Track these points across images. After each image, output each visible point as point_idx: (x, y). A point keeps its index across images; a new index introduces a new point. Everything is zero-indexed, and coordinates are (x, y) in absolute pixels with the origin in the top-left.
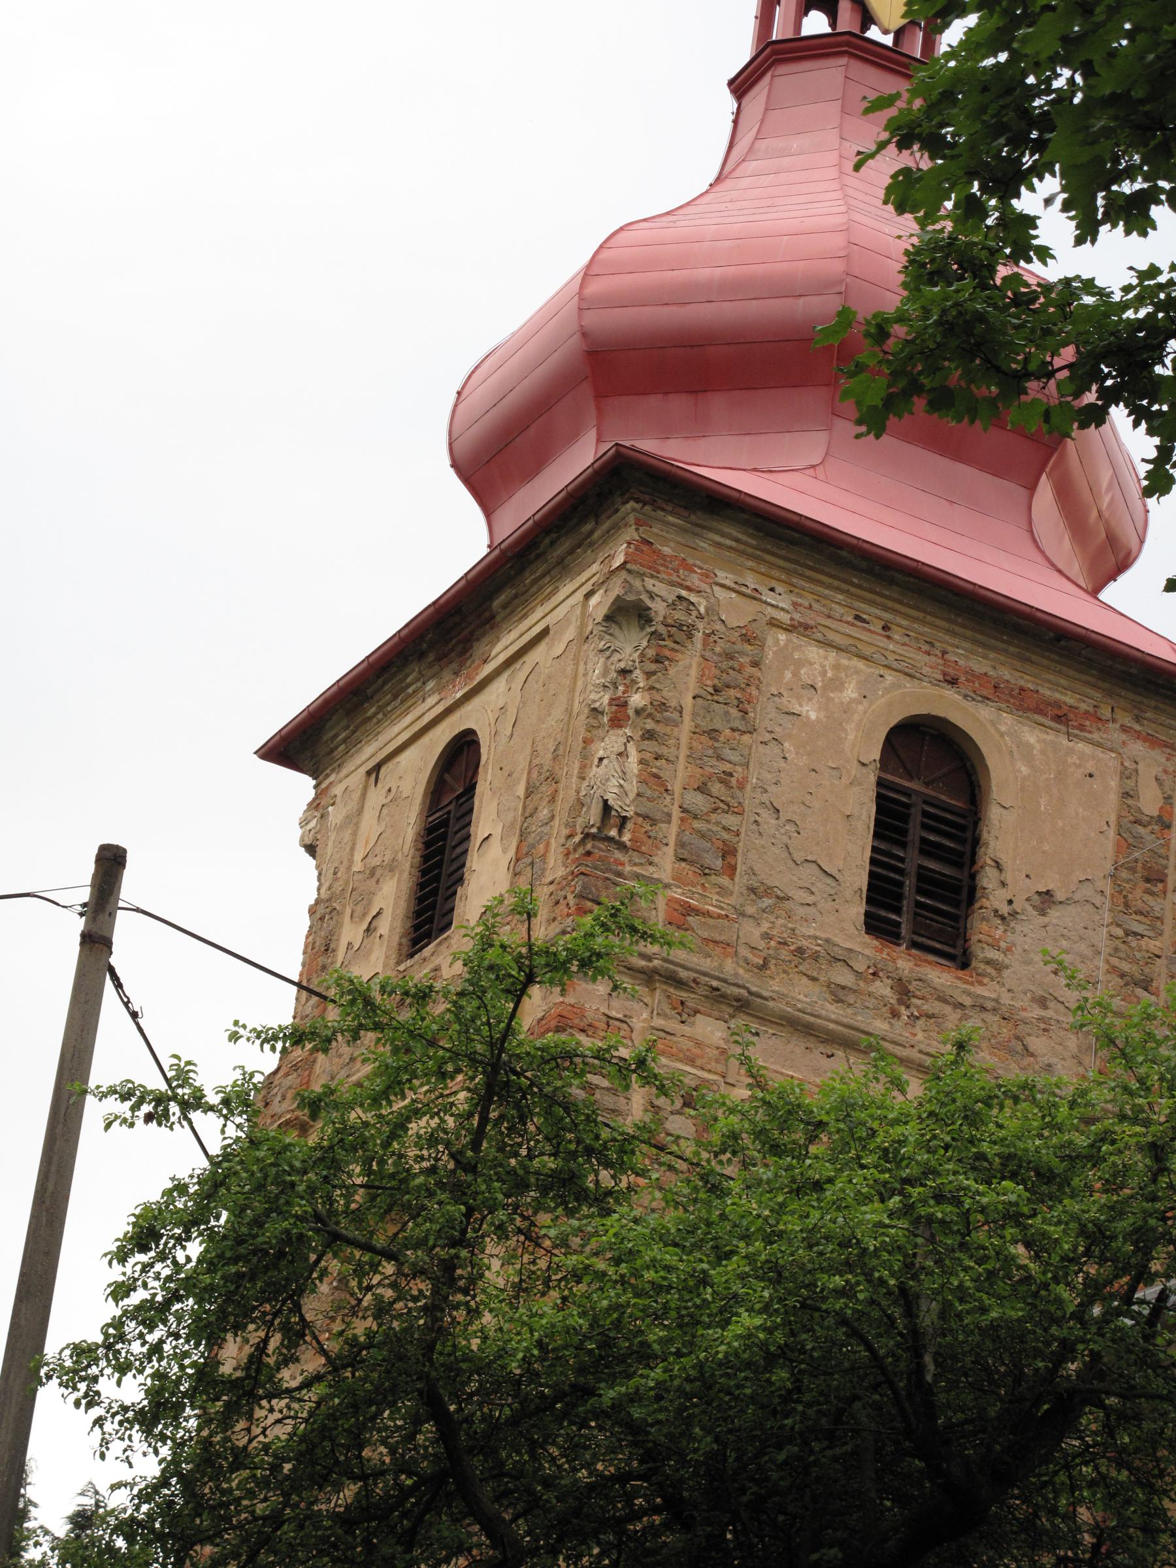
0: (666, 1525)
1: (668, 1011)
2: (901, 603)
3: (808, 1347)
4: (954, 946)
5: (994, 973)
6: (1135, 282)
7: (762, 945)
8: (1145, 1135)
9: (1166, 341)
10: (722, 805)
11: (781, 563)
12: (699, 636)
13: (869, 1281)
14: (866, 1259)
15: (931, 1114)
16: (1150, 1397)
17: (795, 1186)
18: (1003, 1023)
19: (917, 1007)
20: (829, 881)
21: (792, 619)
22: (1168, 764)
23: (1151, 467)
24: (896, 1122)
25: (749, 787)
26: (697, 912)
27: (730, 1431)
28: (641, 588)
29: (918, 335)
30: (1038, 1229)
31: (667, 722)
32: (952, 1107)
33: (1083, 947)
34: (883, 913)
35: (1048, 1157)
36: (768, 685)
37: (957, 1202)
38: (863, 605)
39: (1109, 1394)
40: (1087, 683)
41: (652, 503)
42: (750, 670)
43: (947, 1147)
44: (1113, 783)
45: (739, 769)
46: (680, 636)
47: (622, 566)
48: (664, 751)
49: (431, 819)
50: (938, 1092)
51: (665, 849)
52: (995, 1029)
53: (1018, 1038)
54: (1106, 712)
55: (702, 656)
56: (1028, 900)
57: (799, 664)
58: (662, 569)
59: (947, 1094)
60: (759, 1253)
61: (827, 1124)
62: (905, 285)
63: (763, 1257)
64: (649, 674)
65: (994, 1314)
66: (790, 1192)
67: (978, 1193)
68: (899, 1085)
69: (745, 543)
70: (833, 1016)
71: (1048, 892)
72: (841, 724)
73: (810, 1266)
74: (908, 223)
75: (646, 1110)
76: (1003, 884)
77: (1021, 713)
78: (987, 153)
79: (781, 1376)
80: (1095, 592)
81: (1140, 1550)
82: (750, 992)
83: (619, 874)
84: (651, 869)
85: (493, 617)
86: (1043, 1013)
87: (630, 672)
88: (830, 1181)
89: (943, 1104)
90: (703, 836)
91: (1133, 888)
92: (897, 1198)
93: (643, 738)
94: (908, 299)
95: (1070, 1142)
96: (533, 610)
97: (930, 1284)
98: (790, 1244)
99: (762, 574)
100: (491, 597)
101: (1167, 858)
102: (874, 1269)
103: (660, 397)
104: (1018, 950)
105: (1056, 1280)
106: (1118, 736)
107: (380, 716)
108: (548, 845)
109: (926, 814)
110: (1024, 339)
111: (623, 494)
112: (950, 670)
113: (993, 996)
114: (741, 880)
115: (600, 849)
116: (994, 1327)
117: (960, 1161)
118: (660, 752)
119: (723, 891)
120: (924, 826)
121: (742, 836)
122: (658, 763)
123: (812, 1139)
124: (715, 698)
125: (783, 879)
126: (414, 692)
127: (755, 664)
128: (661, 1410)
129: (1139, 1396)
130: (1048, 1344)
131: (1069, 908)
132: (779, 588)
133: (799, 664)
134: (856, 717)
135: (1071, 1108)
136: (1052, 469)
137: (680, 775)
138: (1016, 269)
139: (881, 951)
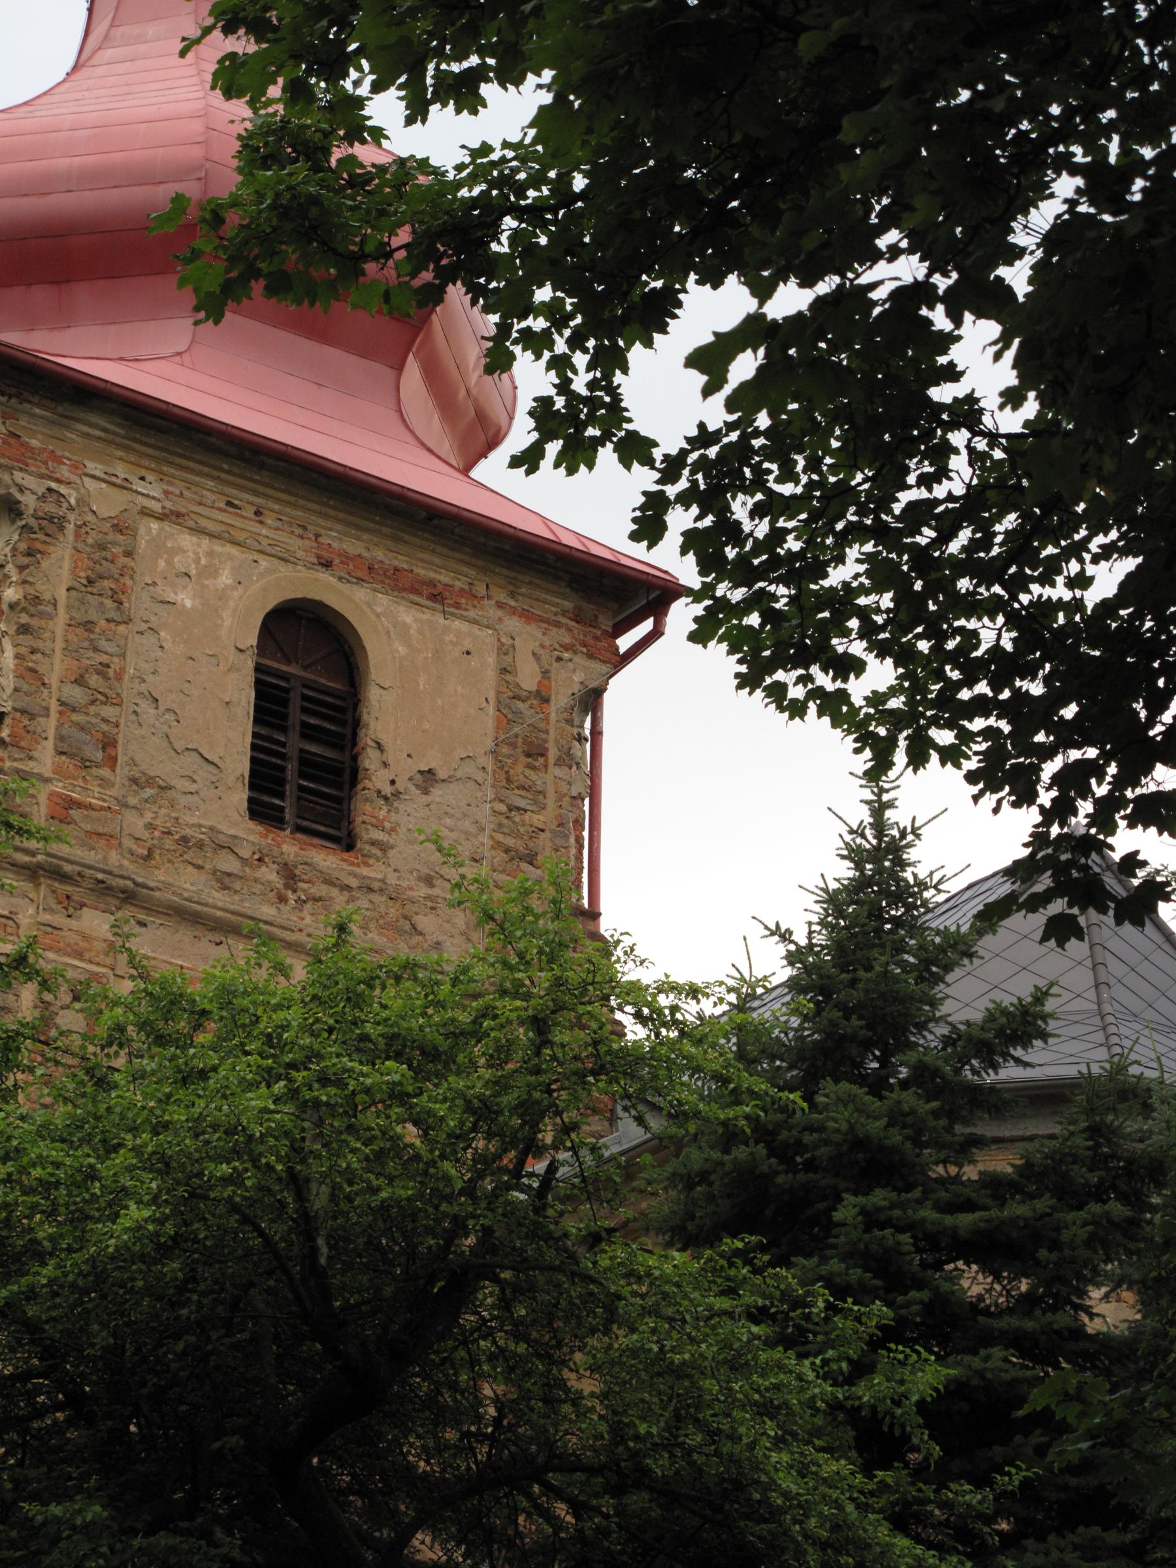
0: (69, 1422)
1: (54, 906)
2: (273, 487)
3: (201, 1236)
4: (338, 829)
5: (379, 853)
6: (467, 160)
7: (146, 835)
8: (526, 1009)
9: (501, 218)
10: (100, 697)
11: (151, 451)
12: (70, 528)
13: (255, 1166)
14: (253, 1146)
15: (315, 997)
16: (542, 1269)
17: (180, 1076)
18: (391, 903)
19: (304, 891)
20: (211, 768)
22: (545, 638)
23: (491, 344)
24: (278, 1007)
25: (126, 677)
26: (79, 805)
27: (127, 1325)
29: (252, 220)
30: (422, 1108)
31: (41, 615)
32: (335, 990)
33: (467, 825)
34: (266, 799)
35: (432, 1036)
36: (143, 574)
37: (340, 1084)
39: (504, 1268)
40: (461, 561)
41: (18, 396)
42: (123, 560)
43: (330, 1030)
44: (491, 660)
45: (116, 660)
46: (51, 529)
48: (39, 644)
50: (320, 976)
51: (44, 743)
52: (383, 910)
53: (406, 917)
54: (481, 590)
55: (75, 548)
56: (410, 779)
57: (173, 552)
59: (330, 977)
60: (145, 1145)
61: (210, 1012)
62: (240, 170)
63: (150, 1149)
64: (21, 568)
65: (384, 1194)
66: (175, 1083)
67: (363, 1075)
68: (282, 969)
69: (114, 433)
70: (220, 904)
71: (430, 771)
73: (197, 1155)
74: (240, 109)
75: (35, 1007)
76: (385, 765)
78: (311, 35)
79: (173, 1267)
80: (466, 470)
81: (542, 1421)
82: (135, 883)
84: (31, 764)
86: (430, 891)
88: (215, 1069)
89: (325, 987)
90: (82, 729)
91: (515, 763)
92: (282, 1083)
94: (243, 184)
95: (453, 1020)
97: (317, 1168)
98: (176, 1134)
101: (547, 732)
102: (261, 1155)
104: (402, 830)
105: (443, 1156)
106: (493, 613)
109: (305, 698)
110: (360, 220)
113: (379, 876)
114: (122, 772)
116: (384, 1206)
117: (344, 1043)
119: (105, 783)
120: (304, 710)
121: (122, 727)
122: (34, 657)
123: (197, 1027)
125: (163, 767)
127: (129, 554)
128: (56, 1307)
129: (534, 1269)
130: (438, 1221)
131: (452, 786)
132: (150, 477)
133: (173, 552)
134: (231, 604)
135: (454, 986)
136: (420, 347)
137: (56, 668)
138: (350, 151)
139: (266, 836)
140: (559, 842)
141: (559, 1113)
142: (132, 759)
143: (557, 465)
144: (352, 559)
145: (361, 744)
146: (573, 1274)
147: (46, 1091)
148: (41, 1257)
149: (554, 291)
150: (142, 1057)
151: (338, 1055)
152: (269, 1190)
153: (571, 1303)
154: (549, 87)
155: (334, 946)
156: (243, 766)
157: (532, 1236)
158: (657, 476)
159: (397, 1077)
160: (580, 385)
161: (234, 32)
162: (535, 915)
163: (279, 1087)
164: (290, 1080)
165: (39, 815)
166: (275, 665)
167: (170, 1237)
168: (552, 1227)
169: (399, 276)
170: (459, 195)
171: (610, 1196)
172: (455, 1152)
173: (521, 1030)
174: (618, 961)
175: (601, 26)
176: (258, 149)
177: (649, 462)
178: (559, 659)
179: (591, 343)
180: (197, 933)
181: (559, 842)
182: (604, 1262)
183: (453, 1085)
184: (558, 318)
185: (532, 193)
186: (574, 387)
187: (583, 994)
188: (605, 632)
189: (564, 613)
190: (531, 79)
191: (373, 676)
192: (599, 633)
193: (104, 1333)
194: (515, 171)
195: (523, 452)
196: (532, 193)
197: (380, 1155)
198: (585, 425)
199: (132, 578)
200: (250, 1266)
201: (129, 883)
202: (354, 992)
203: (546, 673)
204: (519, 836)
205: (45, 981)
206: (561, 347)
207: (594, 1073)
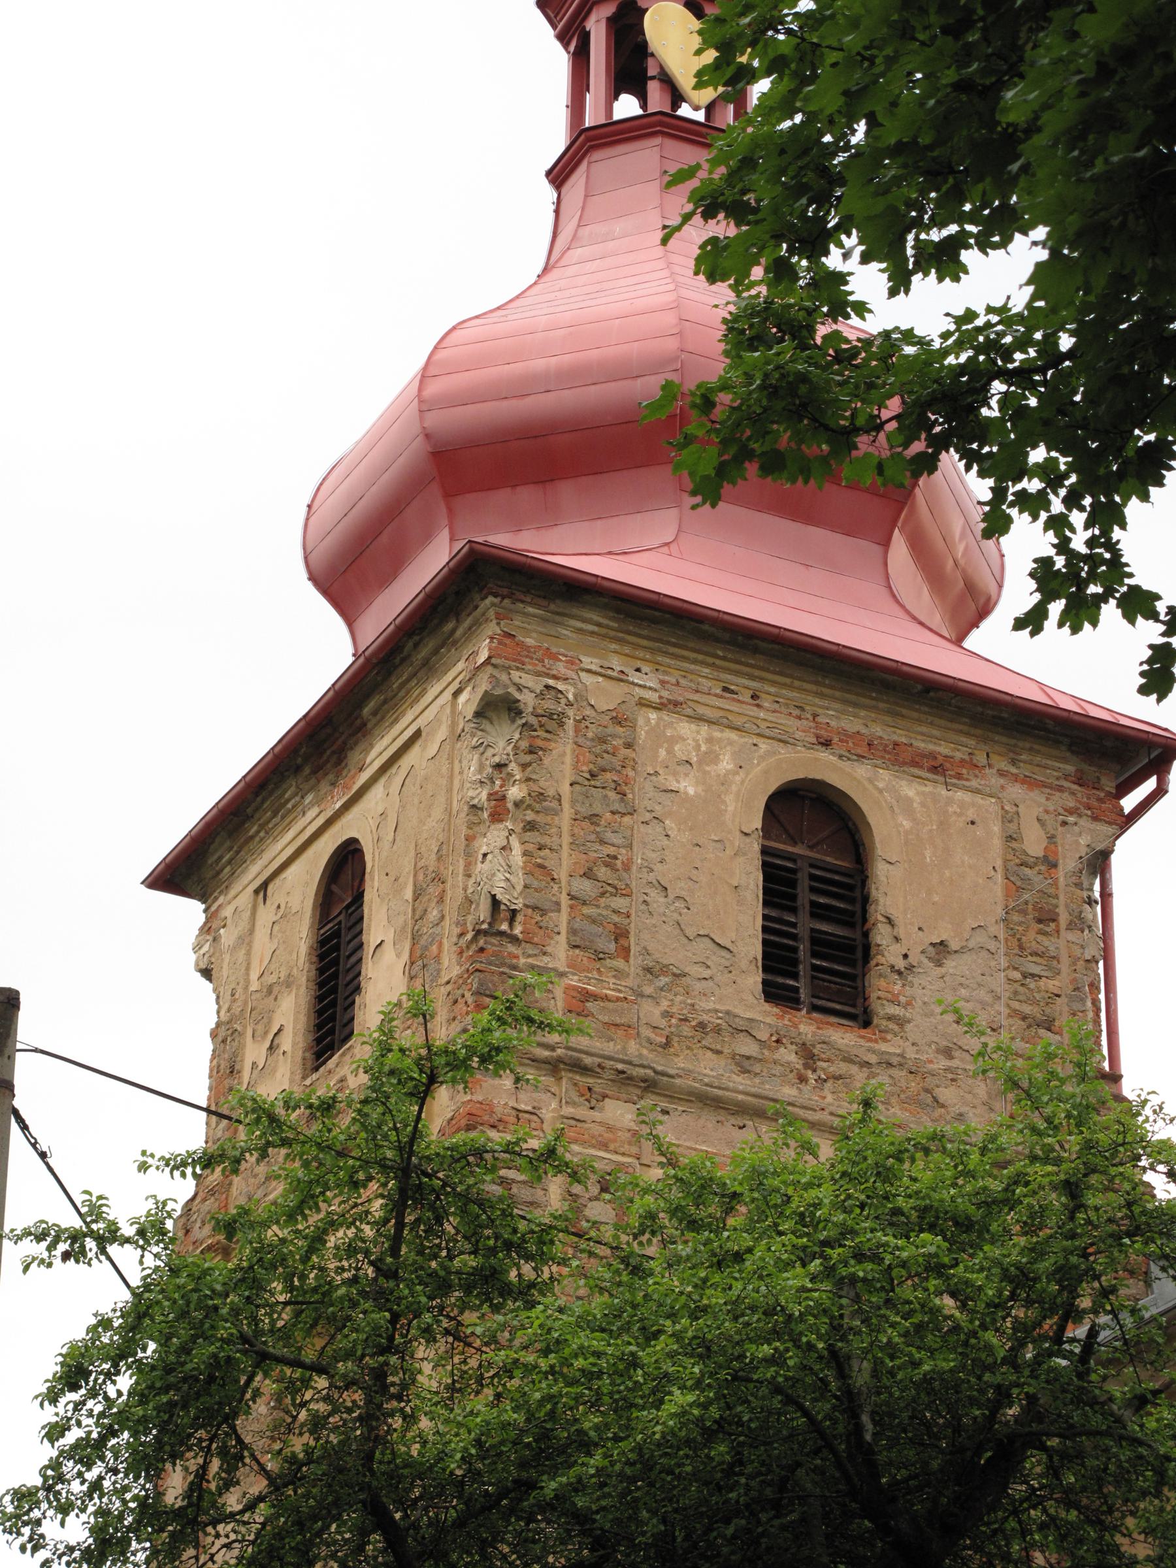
1: (576, 1099)
2: (768, 671)
3: (745, 1419)
4: (854, 1006)
5: (896, 1028)
6: (952, 327)
7: (663, 1023)
9: (989, 383)
10: (609, 889)
11: (645, 643)
12: (570, 723)
14: (793, 1326)
15: (844, 1174)
16: (1091, 1434)
17: (715, 1260)
19: (823, 1069)
20: (724, 953)
21: (661, 697)
22: (1049, 803)
23: (987, 508)
24: (809, 1186)
25: (634, 868)
26: (595, 997)
27: (676, 1511)
28: (508, 682)
31: (547, 811)
33: (982, 994)
34: (780, 980)
35: (965, 1206)
37: (876, 1258)
38: (729, 677)
39: (1049, 1435)
42: (624, 752)
43: (862, 1206)
44: (996, 828)
45: (623, 851)
46: (552, 725)
47: (488, 661)
48: (546, 840)
49: (322, 931)
50: (849, 1152)
51: (557, 938)
52: (903, 1084)
53: (927, 1091)
54: (981, 759)
55: (576, 743)
56: (922, 952)
57: (673, 740)
58: (527, 660)
59: (858, 1153)
60: (685, 1330)
62: (726, 353)
63: (690, 1334)
64: (524, 766)
65: (926, 1368)
66: (711, 1266)
67: (898, 1249)
68: (809, 1148)
69: (607, 627)
70: (741, 1087)
71: (942, 943)
72: (719, 796)
73: (737, 1338)
74: (723, 292)
76: (897, 939)
77: (897, 768)
78: (791, 214)
79: (720, 1450)
80: (959, 640)
82: (656, 1072)
83: (515, 968)
84: (546, 959)
85: (365, 725)
86: (948, 1063)
87: (505, 765)
88: (750, 1250)
89: (854, 1163)
90: (594, 921)
92: (818, 1262)
93: (525, 830)
94: (731, 367)
95: (985, 1188)
96: (403, 713)
97: (859, 1344)
98: (716, 1318)
99: (627, 655)
100: (360, 706)
101: (1056, 897)
102: (801, 1334)
103: (509, 489)
105: (984, 1327)
106: (995, 781)
107: (262, 834)
108: (440, 944)
109: (812, 877)
111: (481, 590)
112: (823, 732)
113: (898, 1051)
114: (636, 961)
115: (494, 945)
116: (927, 1379)
117: (877, 1218)
118: (542, 842)
119: (619, 974)
120: (813, 890)
122: (542, 853)
123: (729, 1210)
124: (593, 783)
125: (676, 955)
126: (293, 807)
127: (629, 746)
128: (604, 1496)
129: (1080, 1435)
130: (982, 1391)
131: (965, 956)
132: (645, 669)
133: (673, 740)
134: (734, 788)
135: (982, 1155)
137: (564, 863)
138: (835, 327)
139: (782, 1017)
140: (1076, 1006)
141: (1097, 1277)
142: (645, 948)
143: (1061, 625)
144: (850, 737)
145: (871, 920)
146: (1121, 1438)
147: (582, 1282)
148: (586, 1445)
149: (1048, 452)
150: (674, 1243)
151: (872, 1231)
152: (811, 1369)
153: (1120, 1466)
154: (1044, 244)
155: (860, 1121)
156: (755, 949)
157: (1078, 1401)
158: (1162, 628)
159: (933, 1249)
160: (1078, 543)
161: (714, 217)
162: (1059, 1079)
163: (815, 1265)
164: (826, 1258)
165: (557, 1009)
166: (781, 846)
167: (715, 1421)
168: (1097, 1392)
169: (892, 447)
170: (946, 363)
171: (1153, 1357)
172: (994, 1321)
173: (1054, 1195)
174: (1147, 1120)
175: (1093, 179)
176: (743, 331)
177: (1153, 615)
178: (1064, 823)
179: (1087, 501)
180: (720, 1118)
181: (1076, 1006)
182: (1151, 1424)
183: (990, 1254)
184: (1052, 477)
185: (1018, 356)
186: (1073, 545)
187: (1113, 1156)
188: (1109, 794)
189: (1066, 777)
190: (1020, 241)
191: (879, 852)
192: (1102, 795)
193: (655, 1521)
194: (1001, 335)
195: (1027, 614)
196: (1018, 356)
197: (919, 1327)
198: (1085, 583)
199: (634, 769)
200: (796, 1446)
201: (650, 1072)
202: (884, 1166)
203: (1051, 838)
204: (1036, 1003)
205: (576, 1173)
206: (1057, 506)
207: (1129, 1235)
